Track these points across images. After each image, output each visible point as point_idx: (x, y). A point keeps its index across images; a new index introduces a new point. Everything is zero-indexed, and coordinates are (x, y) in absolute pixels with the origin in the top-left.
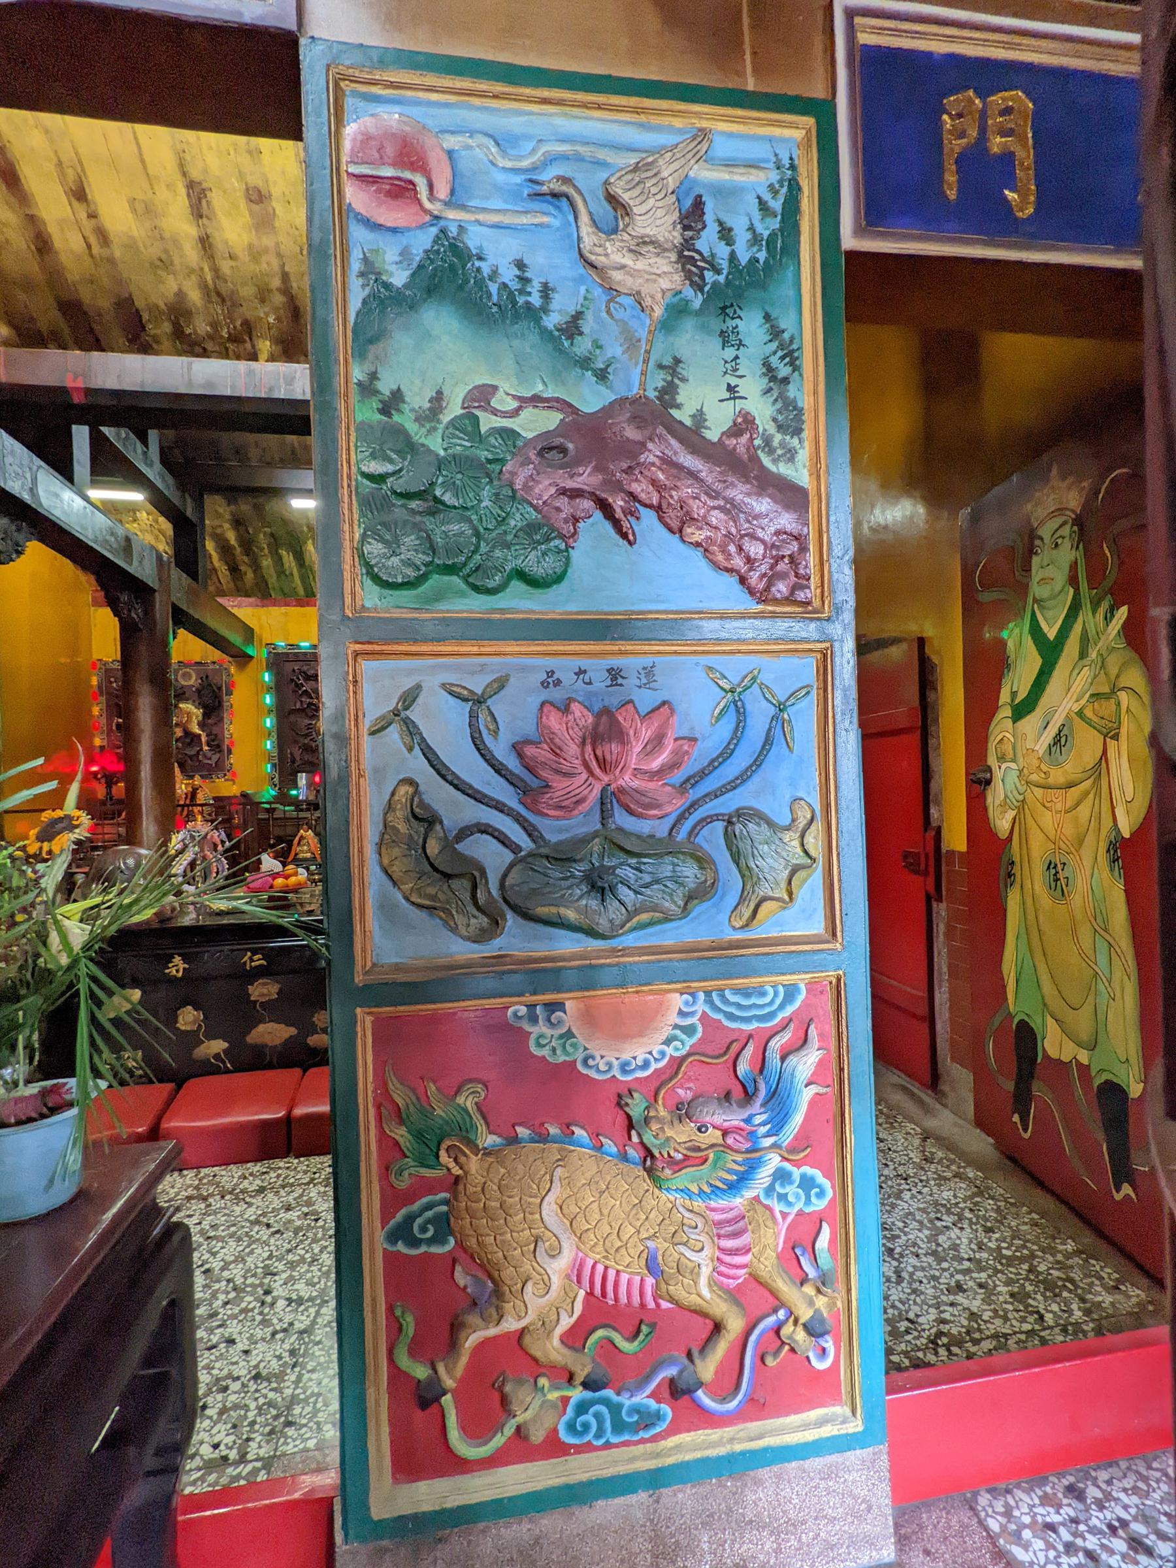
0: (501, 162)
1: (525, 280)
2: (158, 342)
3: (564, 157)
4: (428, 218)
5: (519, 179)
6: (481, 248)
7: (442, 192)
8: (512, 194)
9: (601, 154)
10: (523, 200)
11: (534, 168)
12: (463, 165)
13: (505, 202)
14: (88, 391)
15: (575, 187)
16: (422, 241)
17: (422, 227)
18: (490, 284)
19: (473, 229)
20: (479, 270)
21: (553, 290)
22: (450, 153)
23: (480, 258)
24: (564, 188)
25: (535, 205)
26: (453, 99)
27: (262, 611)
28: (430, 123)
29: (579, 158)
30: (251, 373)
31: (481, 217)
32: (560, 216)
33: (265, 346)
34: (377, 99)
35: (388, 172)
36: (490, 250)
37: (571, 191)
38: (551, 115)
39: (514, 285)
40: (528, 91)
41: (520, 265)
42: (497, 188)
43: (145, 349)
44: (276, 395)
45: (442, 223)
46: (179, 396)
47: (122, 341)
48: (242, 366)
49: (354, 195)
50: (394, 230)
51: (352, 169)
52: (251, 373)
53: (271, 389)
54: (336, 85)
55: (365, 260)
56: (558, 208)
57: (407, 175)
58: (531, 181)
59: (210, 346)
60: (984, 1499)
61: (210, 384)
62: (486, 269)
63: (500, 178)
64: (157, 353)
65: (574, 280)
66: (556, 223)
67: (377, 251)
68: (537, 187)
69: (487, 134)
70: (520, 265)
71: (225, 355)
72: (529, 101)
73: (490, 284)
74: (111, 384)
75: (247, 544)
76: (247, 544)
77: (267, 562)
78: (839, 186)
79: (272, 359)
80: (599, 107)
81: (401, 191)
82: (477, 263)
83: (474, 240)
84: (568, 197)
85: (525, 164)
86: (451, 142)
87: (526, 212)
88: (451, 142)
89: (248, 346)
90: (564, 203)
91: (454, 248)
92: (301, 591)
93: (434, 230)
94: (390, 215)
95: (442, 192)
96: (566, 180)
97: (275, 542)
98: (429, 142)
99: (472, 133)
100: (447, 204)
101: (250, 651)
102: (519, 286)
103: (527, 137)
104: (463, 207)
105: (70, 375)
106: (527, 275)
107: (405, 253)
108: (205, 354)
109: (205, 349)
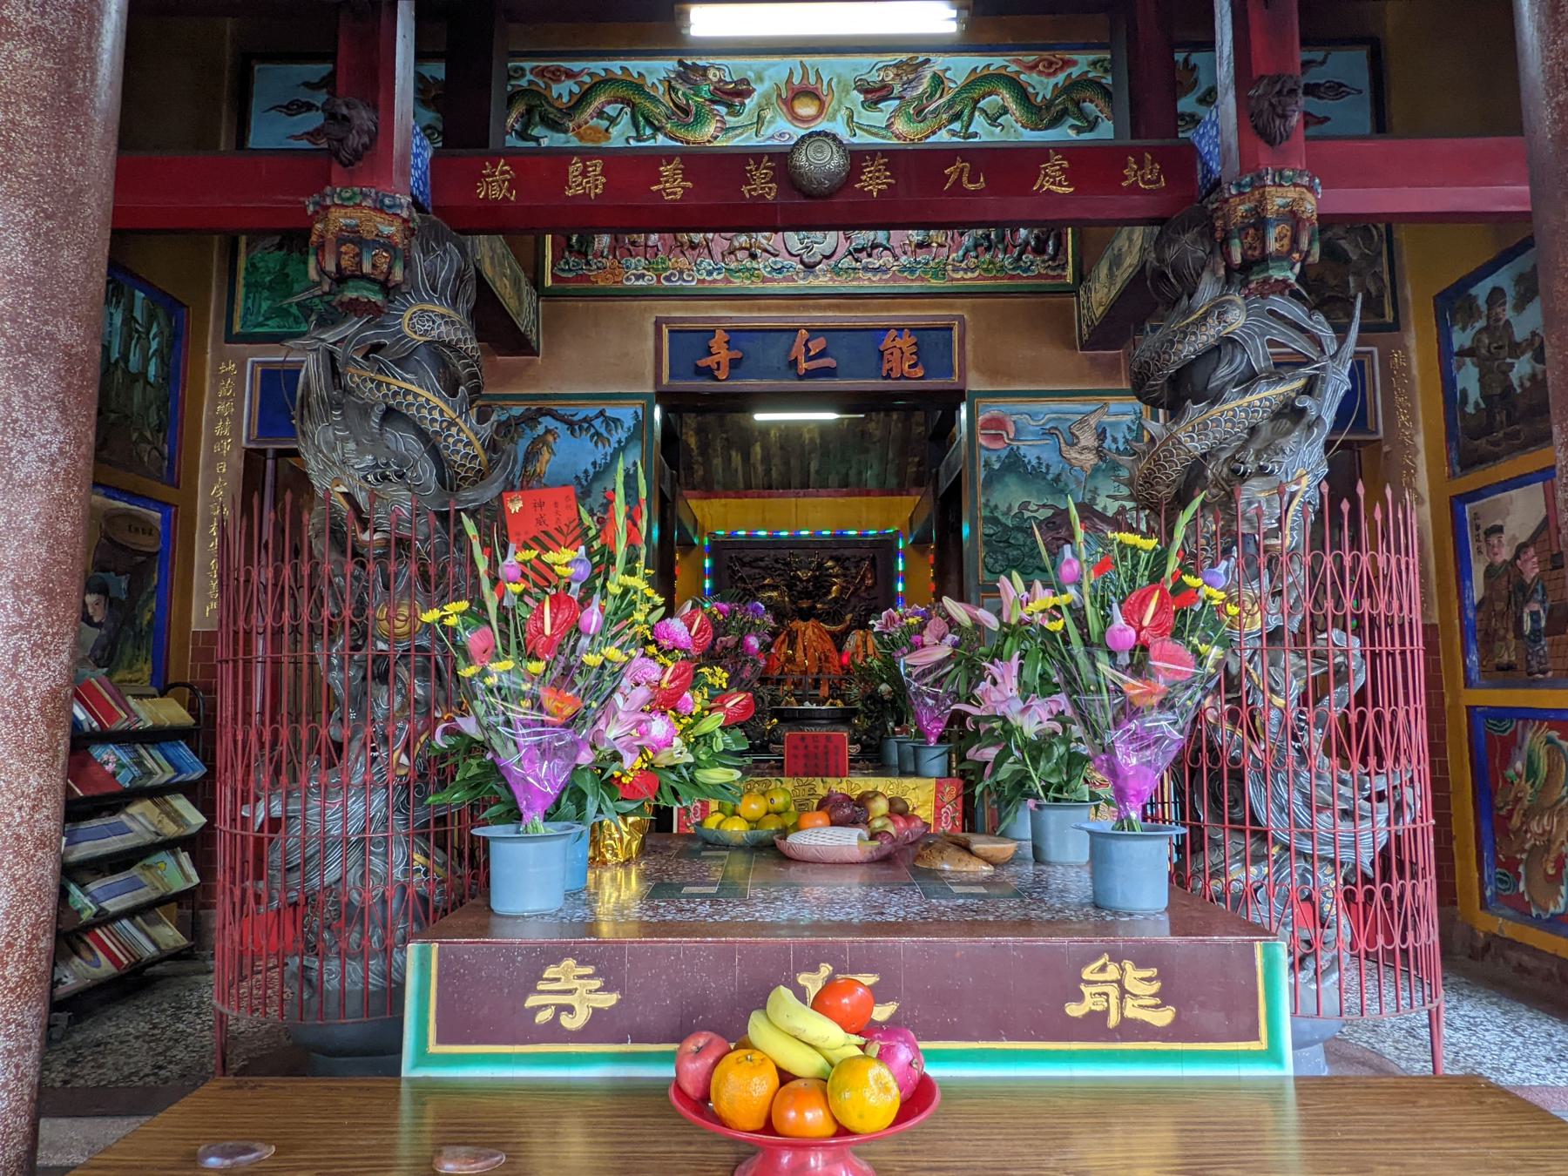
27: (705, 503)
75: (704, 447)
76: (704, 447)
77: (717, 462)
92: (741, 485)
97: (729, 444)
101: (696, 541)
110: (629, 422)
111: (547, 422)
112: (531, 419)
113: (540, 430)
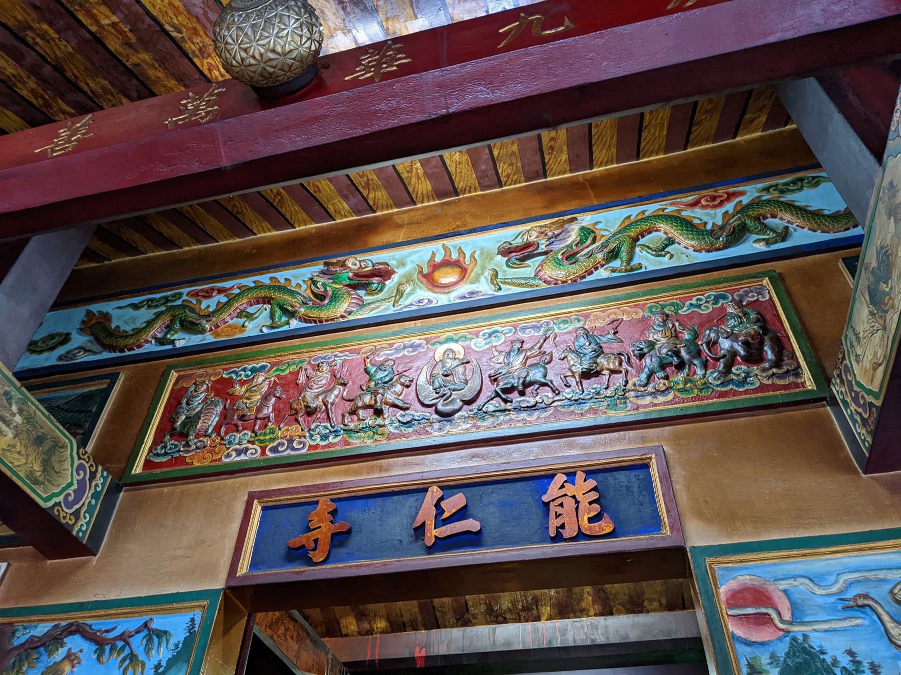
0: (818, 591)
1: (857, 663)
2: (475, 618)
3: (858, 581)
4: (781, 633)
5: (833, 600)
6: (821, 646)
7: (787, 616)
8: (833, 609)
9: (881, 575)
10: (839, 611)
11: (841, 592)
12: (796, 597)
13: (828, 615)
14: (428, 658)
15: (873, 599)
16: (782, 649)
17: (780, 639)
18: (834, 669)
19: (812, 635)
20: (824, 660)
21: (879, 666)
22: (785, 591)
23: (823, 653)
24: (866, 602)
25: (849, 613)
26: (777, 561)
28: (768, 576)
29: (867, 580)
30: (536, 630)
31: (815, 627)
32: (867, 617)
33: (546, 610)
34: (734, 569)
35: (750, 611)
36: (826, 646)
37: (871, 603)
38: (839, 558)
39: (850, 667)
40: (823, 550)
41: (850, 653)
42: (821, 607)
43: (466, 623)
44: (555, 645)
45: (791, 634)
46: (486, 654)
47: (453, 620)
48: (529, 626)
49: (733, 628)
50: (762, 644)
51: (730, 612)
52: (536, 630)
53: (550, 642)
54: (711, 567)
55: (750, 665)
56: (865, 613)
57: (764, 610)
58: (841, 599)
59: (508, 616)
60: (759, 324)
61: (508, 643)
62: (829, 661)
63: (821, 601)
64: (473, 625)
65: (891, 658)
66: (867, 622)
67: (755, 658)
68: (847, 603)
69: (803, 577)
70: (850, 653)
71: (518, 620)
72: (825, 554)
73: (834, 669)
74: (443, 650)
78: (745, 50)
79: (550, 618)
80: (870, 549)
81: (762, 620)
82: (822, 657)
83: (816, 641)
84: (870, 606)
85: (834, 589)
86: (783, 585)
87: (845, 619)
88: (783, 585)
89: (535, 612)
90: (867, 609)
91: (805, 651)
93: (787, 639)
94: (756, 636)
95: (787, 616)
96: (866, 596)
98: (771, 588)
99: (795, 577)
100: (791, 623)
102: (854, 668)
103: (830, 573)
104: (802, 623)
105: (417, 649)
106: (858, 659)
107: (773, 656)
108: (505, 621)
109: (505, 618)
110: (179, 635)
111: (75, 643)
112: (54, 640)
113: (61, 653)
